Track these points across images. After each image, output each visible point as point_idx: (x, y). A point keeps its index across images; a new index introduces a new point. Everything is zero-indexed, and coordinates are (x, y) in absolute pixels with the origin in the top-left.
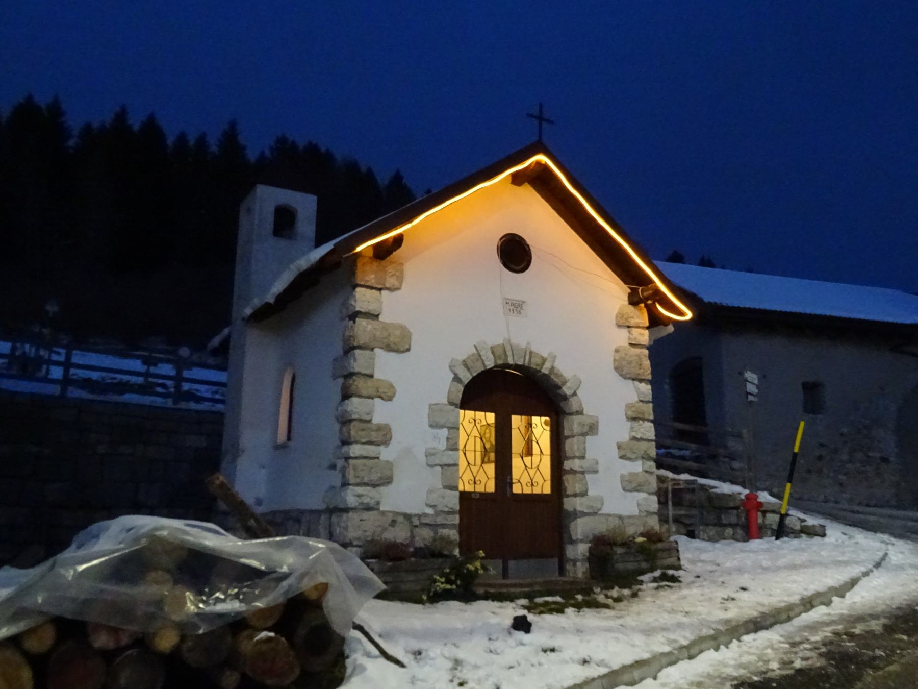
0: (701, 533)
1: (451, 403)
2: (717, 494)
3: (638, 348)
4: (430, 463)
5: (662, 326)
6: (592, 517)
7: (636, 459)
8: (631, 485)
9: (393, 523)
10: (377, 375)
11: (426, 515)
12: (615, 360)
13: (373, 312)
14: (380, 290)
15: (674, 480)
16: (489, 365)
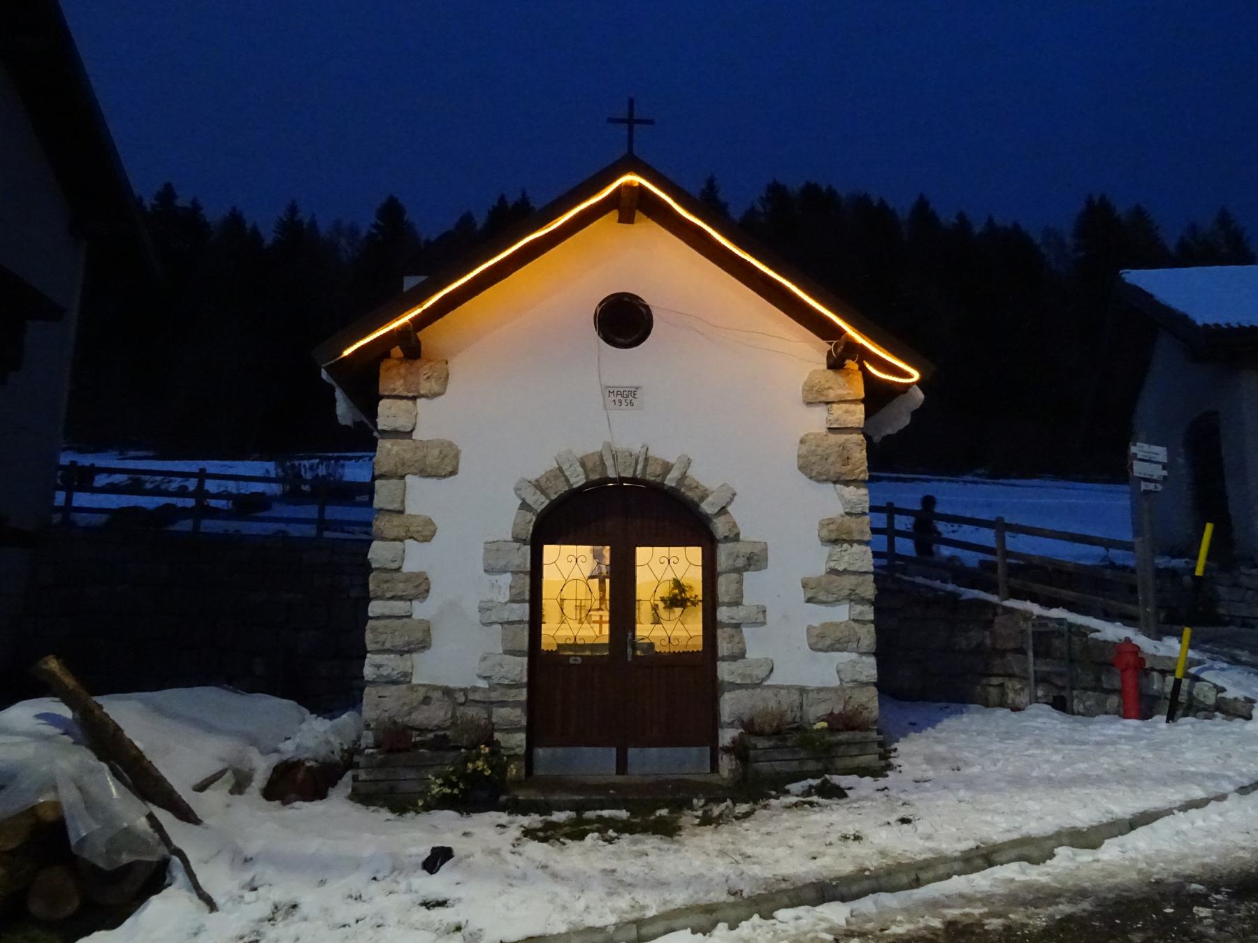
0: (1075, 701)
2: (1096, 640)
4: (484, 621)
5: (902, 396)
6: (750, 690)
7: (837, 601)
8: (823, 641)
9: (426, 700)
10: (410, 509)
12: (799, 456)
13: (401, 429)
14: (414, 398)
15: (1040, 617)
16: (577, 482)
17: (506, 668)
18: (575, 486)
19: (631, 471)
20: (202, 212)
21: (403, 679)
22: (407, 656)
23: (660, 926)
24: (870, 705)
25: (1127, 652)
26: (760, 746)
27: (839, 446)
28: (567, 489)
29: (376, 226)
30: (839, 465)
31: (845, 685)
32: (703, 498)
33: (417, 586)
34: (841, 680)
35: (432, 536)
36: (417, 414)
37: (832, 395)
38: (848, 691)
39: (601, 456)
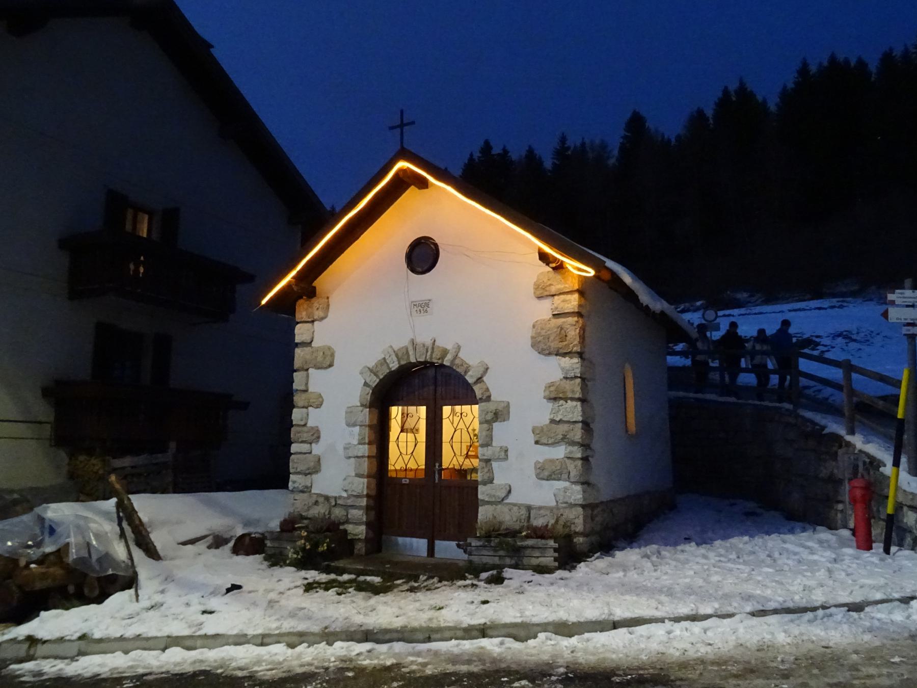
1: (362, 405)
3: (561, 318)
8: (547, 473)
9: (316, 503)
11: (340, 497)
13: (305, 341)
14: (313, 322)
16: (393, 367)
17: (355, 485)
18: (393, 369)
19: (424, 356)
20: (509, 154)
21: (306, 490)
22: (309, 476)
23: (274, 639)
24: (576, 521)
25: (857, 487)
26: (473, 544)
27: (558, 328)
28: (388, 371)
29: (625, 137)
30: (556, 342)
31: (560, 505)
32: (466, 372)
33: (312, 435)
34: (557, 502)
35: (321, 405)
36: (314, 332)
37: (553, 290)
38: (562, 510)
39: (407, 349)
